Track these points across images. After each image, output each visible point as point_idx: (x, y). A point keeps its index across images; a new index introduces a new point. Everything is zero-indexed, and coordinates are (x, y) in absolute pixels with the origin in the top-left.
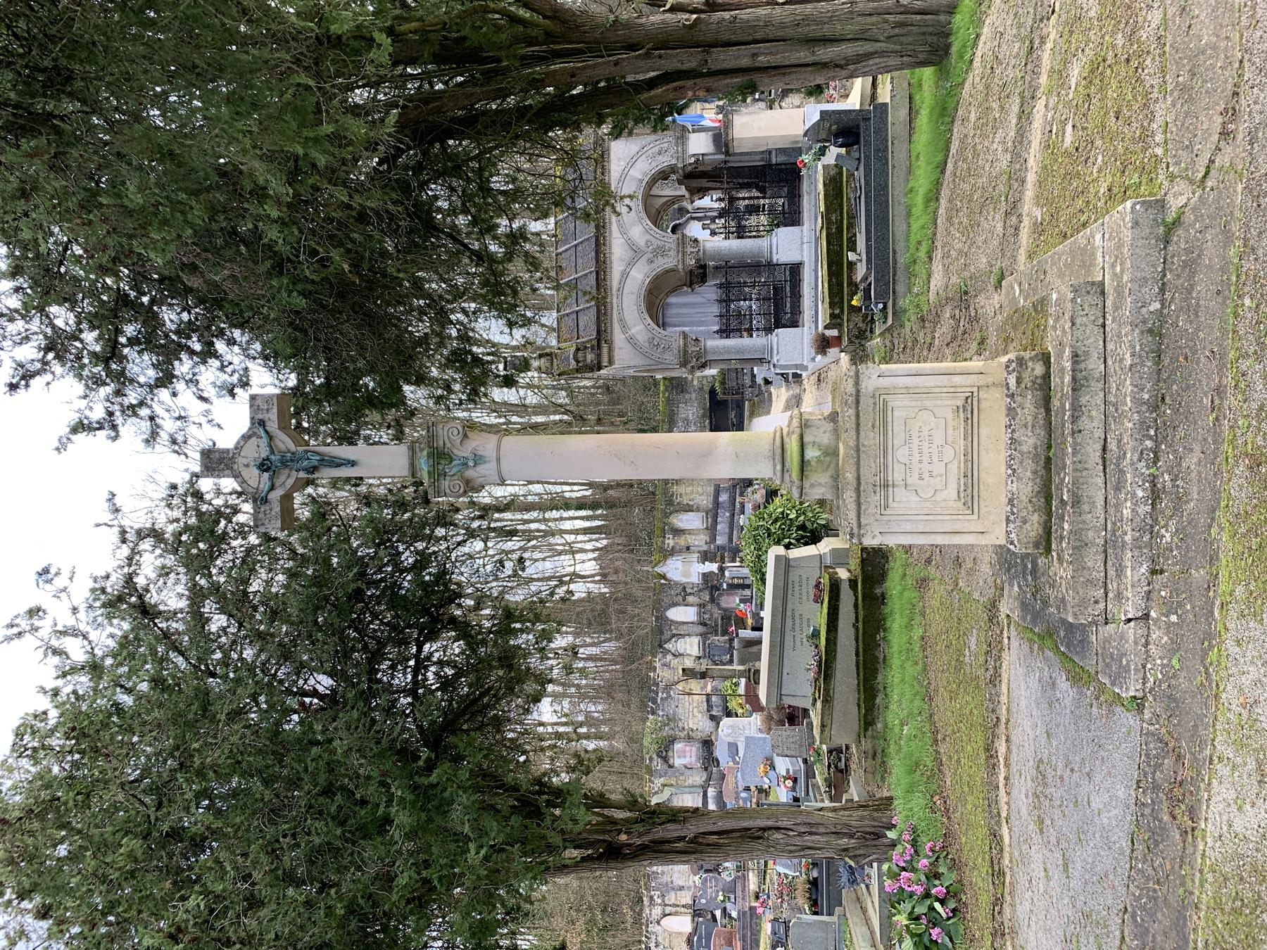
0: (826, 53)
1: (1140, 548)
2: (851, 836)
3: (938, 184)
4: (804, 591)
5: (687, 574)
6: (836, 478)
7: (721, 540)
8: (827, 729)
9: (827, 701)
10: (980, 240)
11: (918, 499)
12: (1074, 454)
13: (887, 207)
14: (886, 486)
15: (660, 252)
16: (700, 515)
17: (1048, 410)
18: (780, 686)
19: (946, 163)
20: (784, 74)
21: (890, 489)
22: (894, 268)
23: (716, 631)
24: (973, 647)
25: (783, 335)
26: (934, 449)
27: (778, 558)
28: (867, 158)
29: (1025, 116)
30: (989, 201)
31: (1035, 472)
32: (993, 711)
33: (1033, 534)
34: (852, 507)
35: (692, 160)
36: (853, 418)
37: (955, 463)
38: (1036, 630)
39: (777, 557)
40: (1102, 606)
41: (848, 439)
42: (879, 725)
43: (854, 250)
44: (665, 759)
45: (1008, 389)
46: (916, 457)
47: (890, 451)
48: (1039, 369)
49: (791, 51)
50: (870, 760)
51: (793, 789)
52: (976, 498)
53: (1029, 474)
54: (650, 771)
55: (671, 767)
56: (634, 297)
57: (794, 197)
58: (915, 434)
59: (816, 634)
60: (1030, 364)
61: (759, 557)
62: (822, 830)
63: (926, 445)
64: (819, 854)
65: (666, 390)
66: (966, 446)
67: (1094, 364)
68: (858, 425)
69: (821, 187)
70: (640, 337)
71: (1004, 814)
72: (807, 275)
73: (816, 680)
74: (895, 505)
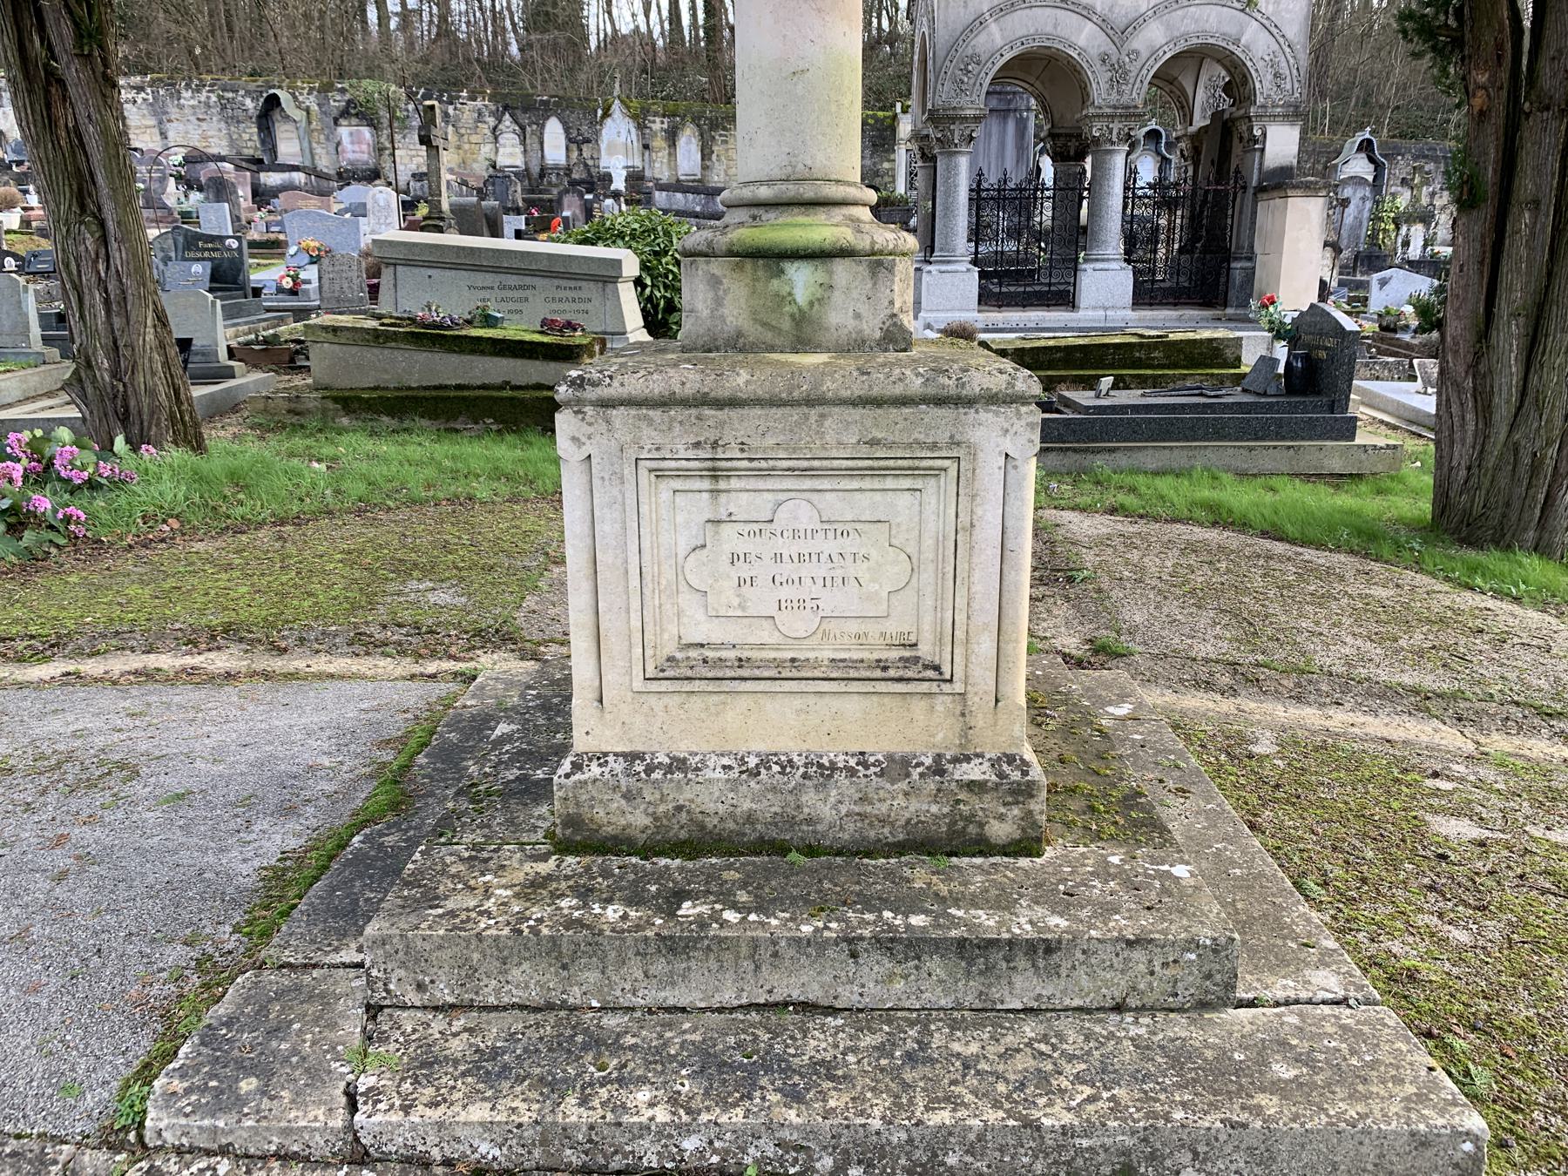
0: (1509, 339)
1: (544, 1142)
2: (115, 374)
3: (1241, 525)
4: (566, 306)
5: (612, 150)
6: (737, 345)
7: (660, 197)
8: (330, 336)
9: (377, 338)
10: (1172, 607)
11: (683, 548)
12: (796, 942)
14: (715, 474)
15: (1119, 75)
16: (698, 171)
17: (899, 849)
18: (409, 263)
19: (1280, 540)
20: (1481, 263)
21: (706, 484)
22: (1086, 450)
23: (532, 191)
24: (432, 598)
25: (969, 281)
26: (809, 590)
27: (617, 264)
28: (1269, 408)
29: (1422, 702)
30: (1250, 629)
31: (750, 818)
32: (302, 640)
33: (600, 813)
34: (656, 386)
35: (1257, 132)
36: (898, 390)
37: (775, 638)
38: (421, 759)
39: (619, 262)
40: (412, 997)
41: (843, 377)
42: (345, 421)
43: (1115, 386)
44: (345, 113)
45: (956, 760)
46: (788, 547)
47: (808, 484)
48: (1001, 831)
49: (1529, 274)
50: (286, 405)
51: (280, 290)
52: (687, 686)
53: (747, 805)
54: (326, 89)
55: (336, 121)
56: (1049, 29)
57: (1174, 297)
58: (849, 545)
59: (489, 321)
60: (1016, 811)
61: (621, 235)
62: (117, 322)
63: (821, 570)
64: (74, 320)
65: (877, 120)
66: (817, 664)
67: (1023, 988)
68: (878, 402)
69: (1206, 334)
70: (982, 38)
71: (91, 667)
72: (1055, 316)
73: (413, 320)
74: (665, 495)
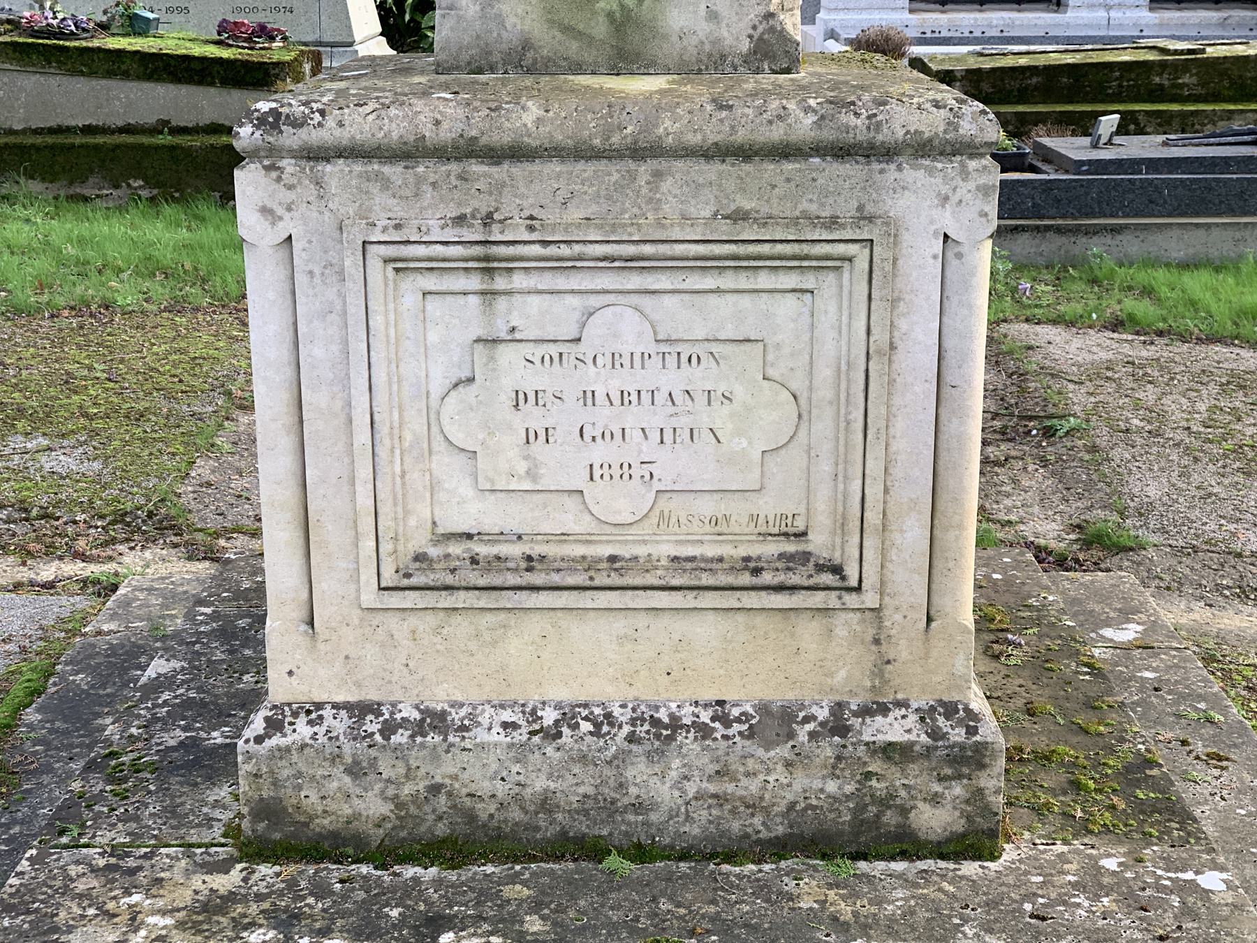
10: (1206, 475)
11: (436, 389)
13: (1232, 212)
17: (778, 849)
22: (1076, 230)
26: (635, 450)
31: (546, 803)
33: (311, 798)
36: (776, 134)
37: (583, 525)
38: (32, 715)
43: (1122, 130)
46: (605, 382)
47: (635, 281)
52: (446, 600)
53: (540, 783)
58: (702, 377)
59: (136, 25)
60: (958, 790)
63: (656, 418)
66: (649, 565)
68: (745, 153)
74: (410, 299)
